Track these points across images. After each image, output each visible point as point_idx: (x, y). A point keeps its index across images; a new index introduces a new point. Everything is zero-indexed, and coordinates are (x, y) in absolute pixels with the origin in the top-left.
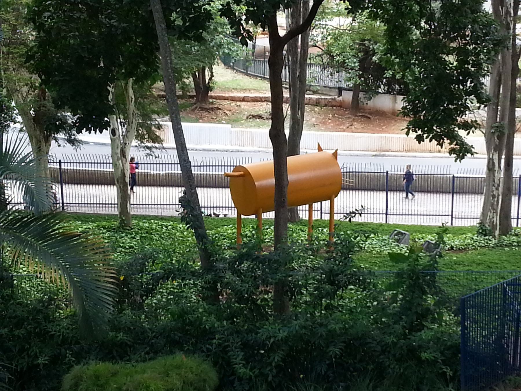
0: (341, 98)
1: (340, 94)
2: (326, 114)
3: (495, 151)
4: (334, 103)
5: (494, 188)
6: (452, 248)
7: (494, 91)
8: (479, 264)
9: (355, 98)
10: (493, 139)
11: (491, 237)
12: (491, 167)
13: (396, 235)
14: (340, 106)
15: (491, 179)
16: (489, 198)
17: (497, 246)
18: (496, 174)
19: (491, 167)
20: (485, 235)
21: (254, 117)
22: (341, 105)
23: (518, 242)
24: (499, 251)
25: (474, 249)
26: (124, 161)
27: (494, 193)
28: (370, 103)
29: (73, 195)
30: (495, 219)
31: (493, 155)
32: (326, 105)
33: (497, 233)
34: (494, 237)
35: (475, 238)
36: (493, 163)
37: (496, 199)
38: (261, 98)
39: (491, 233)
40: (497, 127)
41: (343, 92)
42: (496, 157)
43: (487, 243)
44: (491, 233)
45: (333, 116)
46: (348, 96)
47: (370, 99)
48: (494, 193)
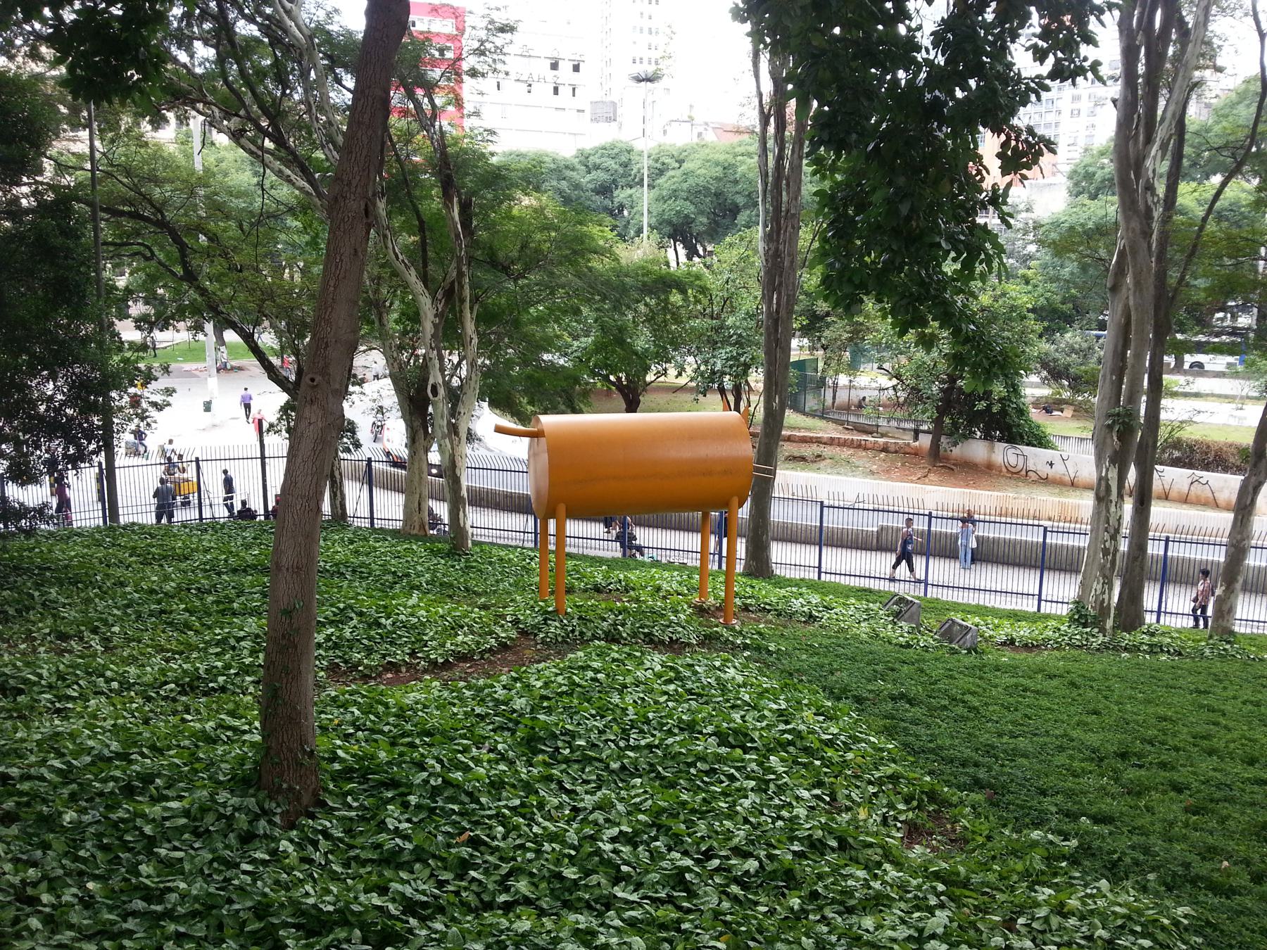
0: (917, 443)
1: (916, 438)
2: (893, 462)
3: (1113, 462)
4: (908, 450)
5: (1107, 536)
6: (1012, 641)
7: (1116, 347)
8: (1051, 677)
9: (935, 444)
10: (1108, 441)
11: (1096, 630)
12: (1102, 494)
13: (896, 603)
14: (916, 454)
15: (1103, 519)
16: (1096, 553)
17: (1107, 648)
18: (1113, 509)
19: (1102, 494)
20: (1085, 626)
21: (795, 458)
22: (916, 453)
23: (1150, 646)
24: (1107, 657)
25: (1057, 649)
26: (456, 442)
27: (1107, 544)
28: (957, 451)
29: (480, 522)
30: (1106, 596)
31: (1107, 470)
32: (896, 452)
33: (1109, 623)
34: (1103, 630)
35: (1063, 628)
36: (1108, 488)
37: (1110, 558)
38: (811, 438)
39: (1098, 622)
40: (1118, 415)
41: (921, 435)
42: (1113, 474)
43: (1087, 639)
44: (1098, 622)
45: (903, 465)
46: (925, 441)
47: (955, 444)
48: (1107, 544)
